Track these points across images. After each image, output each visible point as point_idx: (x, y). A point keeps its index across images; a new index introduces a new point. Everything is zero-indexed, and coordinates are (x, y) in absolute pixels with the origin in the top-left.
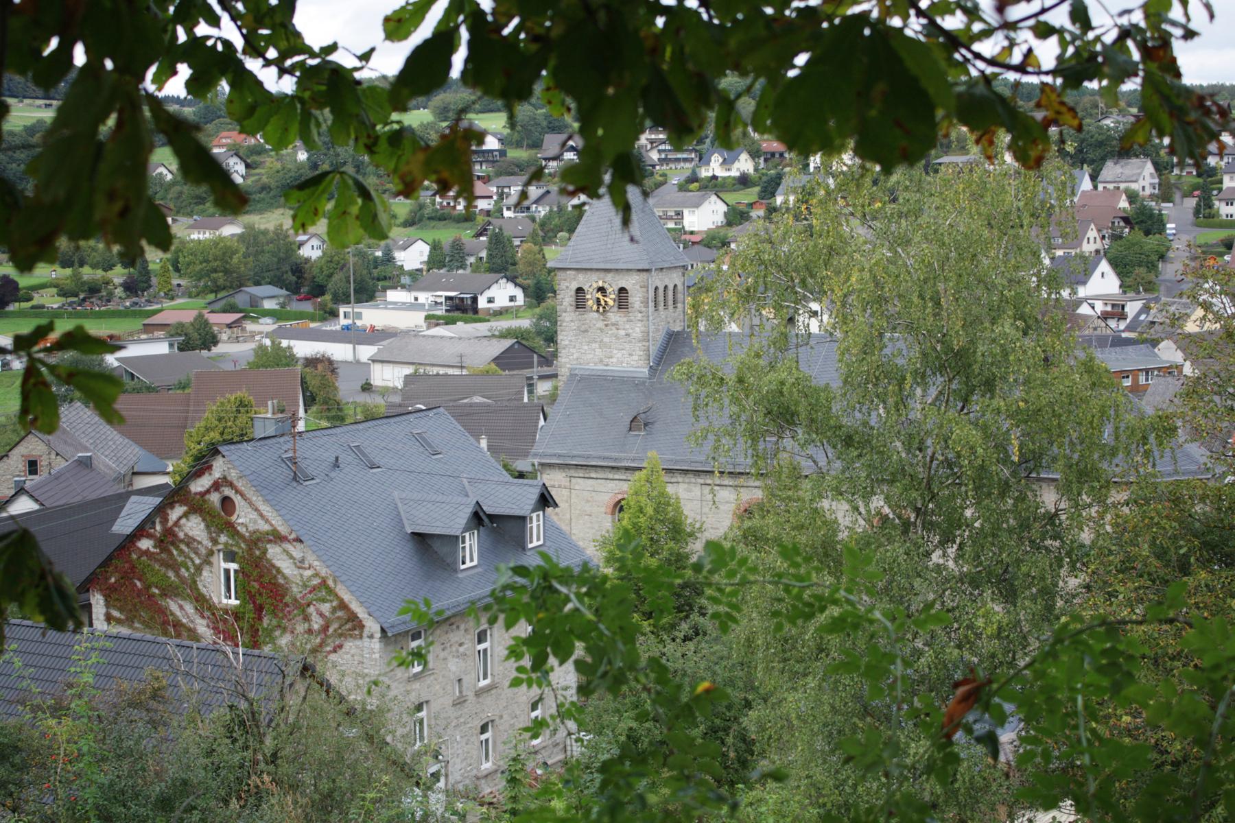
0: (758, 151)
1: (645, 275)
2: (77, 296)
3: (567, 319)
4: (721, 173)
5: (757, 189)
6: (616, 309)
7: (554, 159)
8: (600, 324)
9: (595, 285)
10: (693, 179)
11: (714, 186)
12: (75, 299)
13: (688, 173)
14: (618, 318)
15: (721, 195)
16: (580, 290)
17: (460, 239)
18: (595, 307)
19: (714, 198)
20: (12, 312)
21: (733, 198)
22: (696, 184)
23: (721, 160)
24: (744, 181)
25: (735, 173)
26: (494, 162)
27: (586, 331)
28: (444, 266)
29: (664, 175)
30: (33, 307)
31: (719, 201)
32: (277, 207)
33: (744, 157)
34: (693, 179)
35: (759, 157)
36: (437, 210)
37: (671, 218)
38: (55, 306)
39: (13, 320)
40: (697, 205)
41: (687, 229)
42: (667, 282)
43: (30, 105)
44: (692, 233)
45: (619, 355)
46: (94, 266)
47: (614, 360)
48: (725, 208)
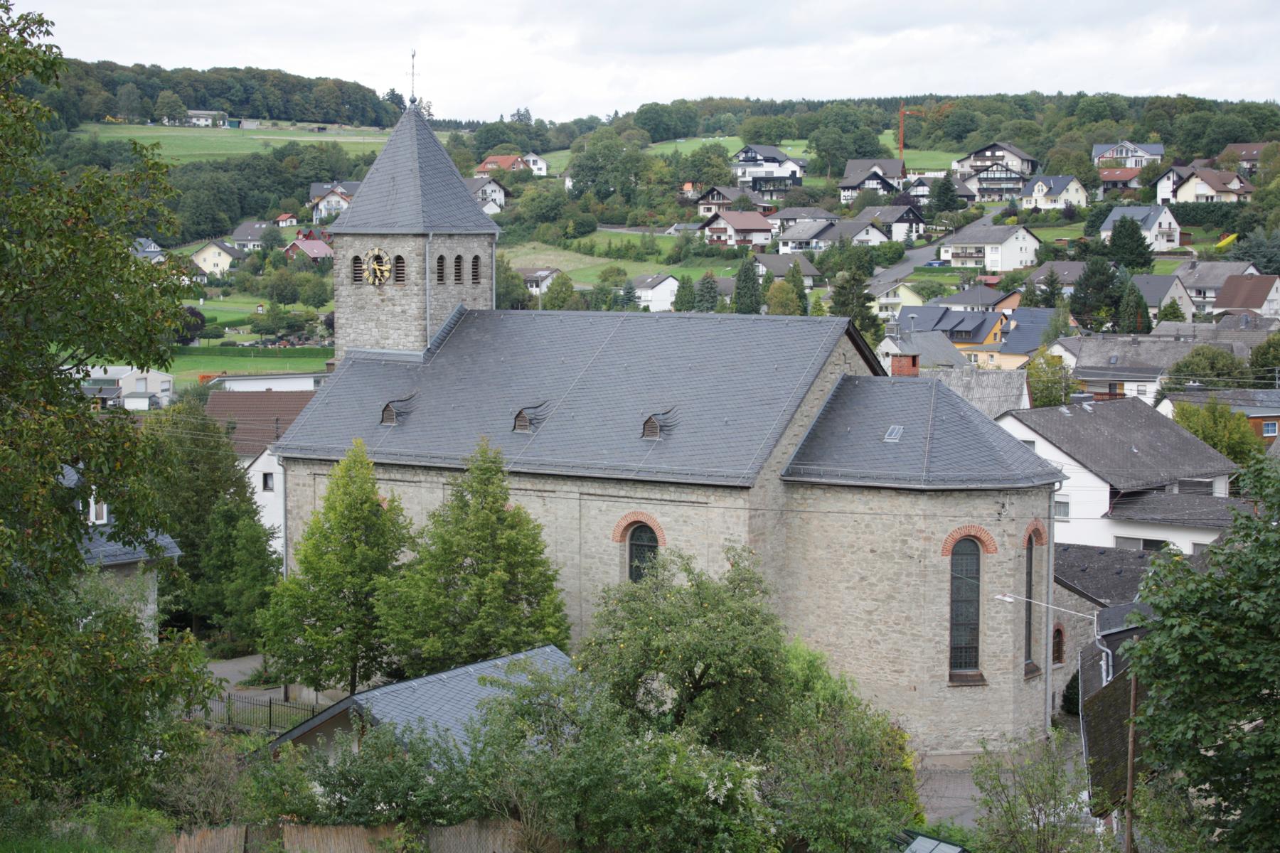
0: (1095, 180)
1: (420, 241)
2: (273, 333)
3: (344, 293)
4: (1044, 205)
5: (1083, 224)
6: (391, 281)
7: (853, 188)
8: (377, 299)
9: (371, 254)
10: (1012, 211)
11: (1032, 221)
12: (272, 337)
13: (1006, 205)
14: (394, 292)
15: (1034, 231)
16: (357, 259)
17: (711, 277)
18: (371, 280)
19: (1022, 232)
20: (197, 349)
21: (1050, 235)
22: (1013, 218)
23: (1045, 190)
24: (1070, 214)
25: (1060, 205)
26: (786, 191)
27: (363, 308)
28: (693, 307)
29: (982, 208)
30: (223, 344)
31: (1029, 237)
32: (530, 241)
33: (1074, 186)
34: (1012, 211)
35: (1097, 187)
36: (705, 245)
37: (970, 256)
38: (246, 344)
39: (195, 358)
40: (1001, 241)
41: (988, 269)
42: (460, 251)
43: (302, 129)
44: (994, 273)
45: (395, 336)
46: (306, 302)
47: (390, 342)
48: (1036, 245)
